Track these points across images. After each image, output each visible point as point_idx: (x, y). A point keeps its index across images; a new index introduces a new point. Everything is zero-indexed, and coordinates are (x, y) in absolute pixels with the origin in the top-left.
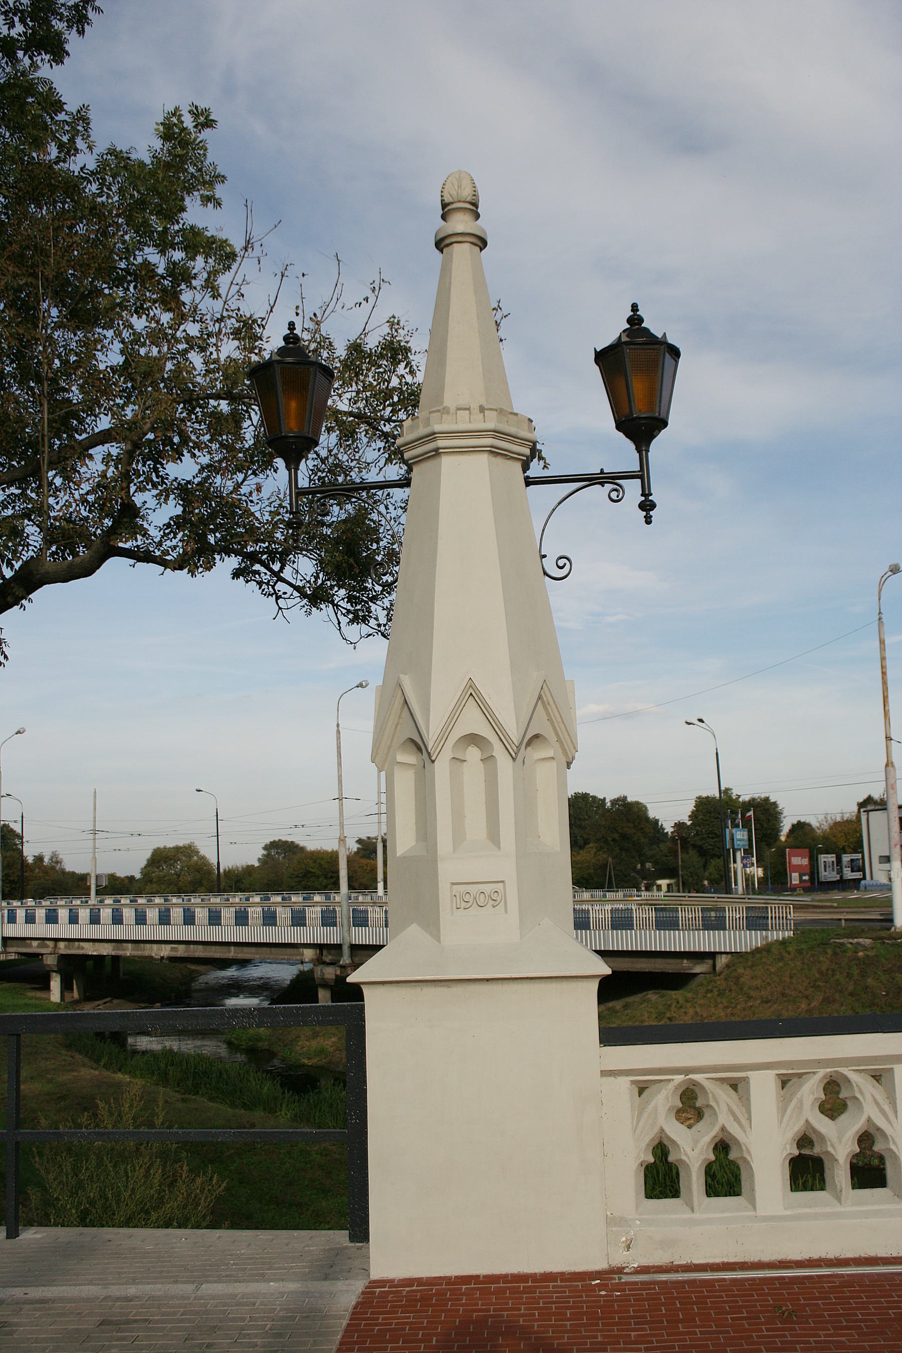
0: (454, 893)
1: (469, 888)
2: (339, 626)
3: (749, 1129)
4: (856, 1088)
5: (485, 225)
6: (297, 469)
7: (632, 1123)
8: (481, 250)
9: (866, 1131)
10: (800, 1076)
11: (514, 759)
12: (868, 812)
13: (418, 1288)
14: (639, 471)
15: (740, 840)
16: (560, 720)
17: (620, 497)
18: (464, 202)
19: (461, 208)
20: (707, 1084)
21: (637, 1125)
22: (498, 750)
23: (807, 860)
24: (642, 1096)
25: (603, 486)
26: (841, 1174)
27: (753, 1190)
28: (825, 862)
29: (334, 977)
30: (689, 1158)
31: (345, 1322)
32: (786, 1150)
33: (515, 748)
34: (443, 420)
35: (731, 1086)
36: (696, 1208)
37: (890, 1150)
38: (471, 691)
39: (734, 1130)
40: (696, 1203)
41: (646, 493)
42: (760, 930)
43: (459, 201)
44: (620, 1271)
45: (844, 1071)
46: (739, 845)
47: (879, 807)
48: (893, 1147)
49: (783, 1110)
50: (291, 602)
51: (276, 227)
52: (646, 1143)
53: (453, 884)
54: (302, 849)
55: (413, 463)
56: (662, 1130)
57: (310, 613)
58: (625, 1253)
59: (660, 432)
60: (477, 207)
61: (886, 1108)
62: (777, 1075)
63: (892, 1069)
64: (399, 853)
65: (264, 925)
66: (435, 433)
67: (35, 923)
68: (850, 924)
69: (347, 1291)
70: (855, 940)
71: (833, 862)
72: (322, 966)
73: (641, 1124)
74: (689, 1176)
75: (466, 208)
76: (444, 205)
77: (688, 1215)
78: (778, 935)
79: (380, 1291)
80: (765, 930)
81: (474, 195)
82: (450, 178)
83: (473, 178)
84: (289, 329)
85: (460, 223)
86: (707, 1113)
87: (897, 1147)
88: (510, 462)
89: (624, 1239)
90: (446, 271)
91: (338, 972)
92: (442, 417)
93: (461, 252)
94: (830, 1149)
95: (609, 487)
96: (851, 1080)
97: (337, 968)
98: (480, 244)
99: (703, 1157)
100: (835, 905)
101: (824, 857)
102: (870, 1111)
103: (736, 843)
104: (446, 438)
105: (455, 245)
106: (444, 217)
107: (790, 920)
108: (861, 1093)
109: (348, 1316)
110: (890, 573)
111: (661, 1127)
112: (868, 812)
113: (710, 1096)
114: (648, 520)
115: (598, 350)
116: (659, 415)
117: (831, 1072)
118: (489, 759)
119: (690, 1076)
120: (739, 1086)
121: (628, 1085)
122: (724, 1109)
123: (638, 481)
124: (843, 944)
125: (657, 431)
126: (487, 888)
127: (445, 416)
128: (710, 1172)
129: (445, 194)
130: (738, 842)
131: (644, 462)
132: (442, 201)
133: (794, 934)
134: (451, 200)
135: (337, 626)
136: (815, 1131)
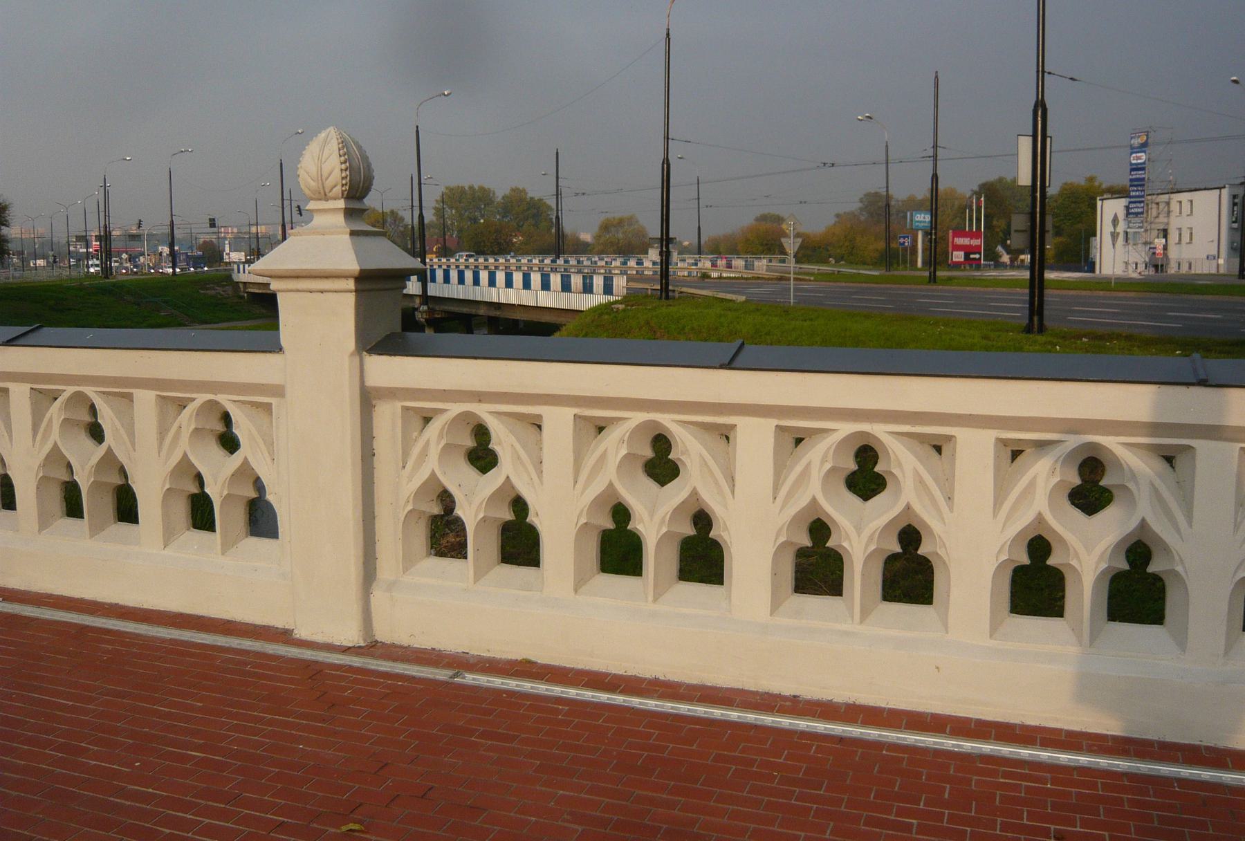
12: (1102, 200)
15: (918, 222)
39: (1159, 527)
47: (1117, 196)
67: (550, 291)
68: (654, 292)
100: (812, 278)
108: (900, 465)
112: (1102, 200)
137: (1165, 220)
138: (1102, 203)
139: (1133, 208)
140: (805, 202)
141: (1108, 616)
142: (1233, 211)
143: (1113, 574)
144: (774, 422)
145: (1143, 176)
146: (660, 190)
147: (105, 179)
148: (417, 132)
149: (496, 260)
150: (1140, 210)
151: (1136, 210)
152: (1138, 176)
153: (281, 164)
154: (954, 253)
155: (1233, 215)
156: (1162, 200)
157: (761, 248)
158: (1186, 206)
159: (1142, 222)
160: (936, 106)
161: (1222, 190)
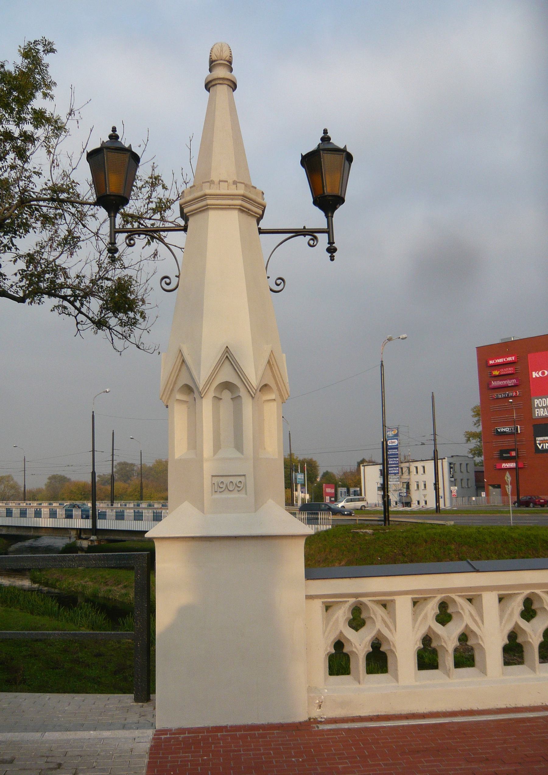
1: (222, 479)
2: (112, 341)
4: (459, 607)
5: (237, 74)
6: (115, 217)
7: (323, 628)
8: (233, 91)
10: (425, 599)
12: (364, 466)
14: (327, 229)
15: (299, 479)
16: (279, 376)
17: (314, 244)
18: (224, 60)
20: (370, 604)
21: (326, 630)
22: (243, 392)
23: (334, 490)
25: (305, 237)
26: (448, 660)
27: (397, 670)
28: (341, 491)
30: (357, 650)
31: (146, 760)
33: (254, 391)
34: (211, 188)
36: (361, 681)
37: (479, 644)
39: (386, 632)
41: (331, 242)
42: (314, 524)
43: (221, 60)
44: (316, 721)
45: (453, 596)
46: (299, 481)
48: (481, 642)
49: (415, 620)
50: (85, 327)
51: (88, 102)
53: (213, 476)
54: (69, 480)
55: (190, 215)
56: (341, 632)
57: (97, 333)
58: (318, 710)
60: (231, 65)
61: (477, 618)
63: (481, 594)
66: (206, 195)
69: (142, 737)
71: (345, 492)
72: (81, 540)
73: (328, 629)
74: (357, 663)
76: (212, 62)
77: (357, 686)
78: (323, 528)
79: (164, 738)
80: (317, 525)
81: (231, 57)
82: (215, 46)
84: (112, 131)
85: (221, 72)
86: (368, 623)
87: (483, 643)
88: (250, 218)
89: (318, 701)
90: (211, 103)
91: (90, 544)
93: (222, 90)
94: (443, 644)
95: (308, 237)
97: (89, 541)
98: (233, 87)
101: (341, 489)
103: (298, 480)
104: (213, 199)
105: (218, 85)
106: (210, 70)
107: (330, 520)
108: (462, 609)
109: (147, 756)
110: (387, 341)
111: (341, 631)
113: (371, 611)
115: (304, 154)
118: (236, 399)
119: (360, 599)
120: (387, 606)
121: (321, 604)
122: (380, 619)
123: (326, 235)
124: (357, 533)
126: (235, 480)
127: (212, 185)
128: (369, 657)
130: (299, 480)
131: (330, 224)
132: (211, 59)
133: (332, 527)
134: (216, 58)
135: (111, 341)
136: (434, 633)
137: (408, 477)
141: (386, 673)
142: (450, 471)
143: (369, 652)
145: (397, 452)
147: (141, 452)
149: (50, 504)
150: (396, 471)
151: (393, 472)
152: (393, 453)
154: (326, 497)
155: (450, 473)
156: (405, 466)
157: (80, 497)
158: (420, 470)
159: (398, 478)
161: (444, 460)
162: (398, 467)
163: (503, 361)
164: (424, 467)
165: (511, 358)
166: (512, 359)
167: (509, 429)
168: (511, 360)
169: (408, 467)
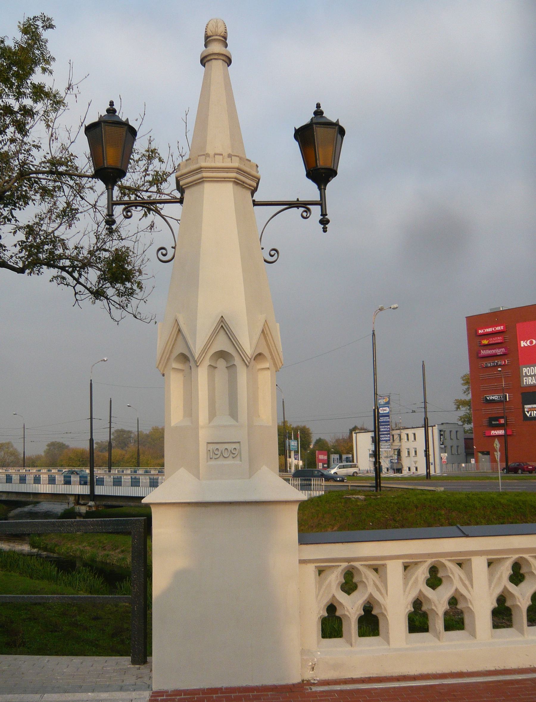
0: (209, 449)
1: (218, 446)
2: (110, 311)
3: (386, 596)
4: (449, 571)
5: (232, 49)
6: (113, 189)
7: (316, 592)
8: (228, 66)
9: (453, 596)
10: (416, 563)
11: (247, 366)
13: (185, 697)
15: (293, 446)
16: (273, 345)
18: (219, 36)
19: (217, 39)
20: (361, 569)
22: (237, 361)
23: (326, 456)
24: (321, 575)
25: (298, 209)
26: (439, 623)
27: (388, 633)
28: (334, 458)
29: (85, 512)
30: (350, 614)
32: (408, 609)
33: (249, 360)
34: (207, 161)
35: (374, 569)
36: (353, 644)
38: (222, 324)
39: (377, 596)
40: (353, 641)
41: (324, 214)
44: (309, 683)
45: (443, 560)
46: (292, 448)
47: (364, 431)
48: (470, 606)
50: (83, 297)
52: (324, 605)
54: (67, 447)
56: (334, 596)
57: (95, 303)
58: (311, 672)
59: (332, 178)
60: (226, 40)
61: (467, 582)
62: (315, 566)
64: (173, 424)
65: (49, 484)
70: (356, 496)
71: (338, 458)
75: (219, 40)
76: (207, 37)
78: (316, 493)
81: (226, 32)
83: (225, 22)
84: (110, 105)
85: (216, 48)
89: (311, 664)
91: (88, 509)
92: (206, 159)
93: (217, 65)
94: (434, 607)
95: (302, 209)
96: (446, 566)
98: (228, 62)
99: (358, 613)
101: (333, 456)
102: (457, 584)
103: (291, 447)
105: (213, 60)
106: (206, 46)
107: (323, 486)
108: (452, 573)
111: (334, 595)
114: (325, 229)
115: (297, 128)
116: (334, 167)
117: (435, 561)
118: (231, 367)
119: (352, 563)
121: (314, 568)
122: (372, 583)
123: (319, 207)
124: (350, 498)
125: (331, 178)
126: (230, 447)
127: (207, 158)
128: (361, 620)
129: (209, 31)
132: (206, 34)
133: (324, 493)
134: (211, 34)
135: (109, 311)
136: (425, 596)
137: (399, 444)
138: (356, 435)
139: (383, 437)
140: (34, 441)
142: (441, 438)
144: (402, 561)
145: (389, 420)
146: (373, 418)
148: (91, 384)
150: (387, 439)
151: (385, 439)
152: (385, 420)
153: (111, 401)
155: (441, 440)
158: (411, 437)
159: (389, 445)
160: (375, 374)
162: (389, 434)
163: (492, 330)
164: (414, 434)
165: (500, 327)
166: (501, 328)
167: (498, 397)
168: (500, 329)
169: (399, 434)
